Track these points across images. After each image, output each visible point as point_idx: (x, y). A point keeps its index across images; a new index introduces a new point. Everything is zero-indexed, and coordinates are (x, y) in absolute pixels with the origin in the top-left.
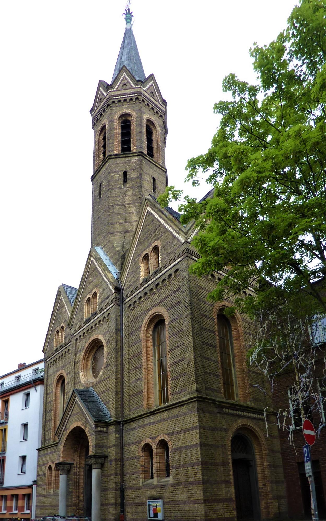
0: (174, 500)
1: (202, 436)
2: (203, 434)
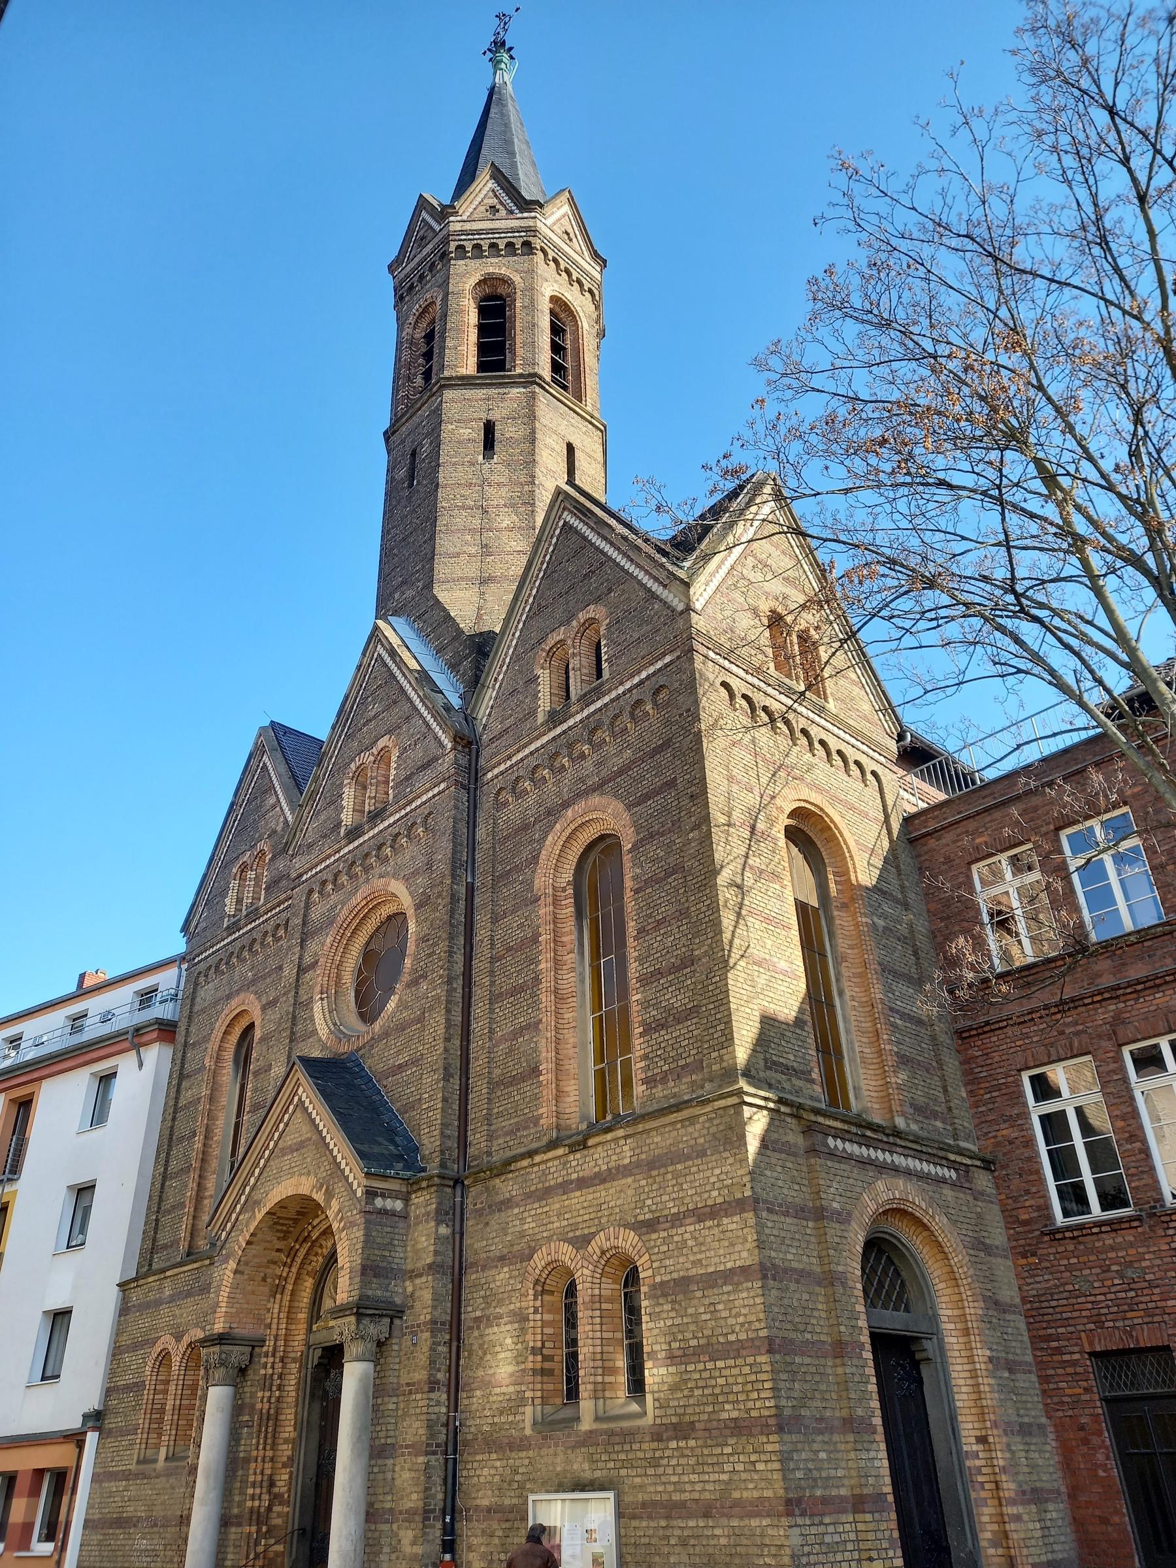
0: (665, 1497)
1: (764, 1238)
2: (767, 1231)
